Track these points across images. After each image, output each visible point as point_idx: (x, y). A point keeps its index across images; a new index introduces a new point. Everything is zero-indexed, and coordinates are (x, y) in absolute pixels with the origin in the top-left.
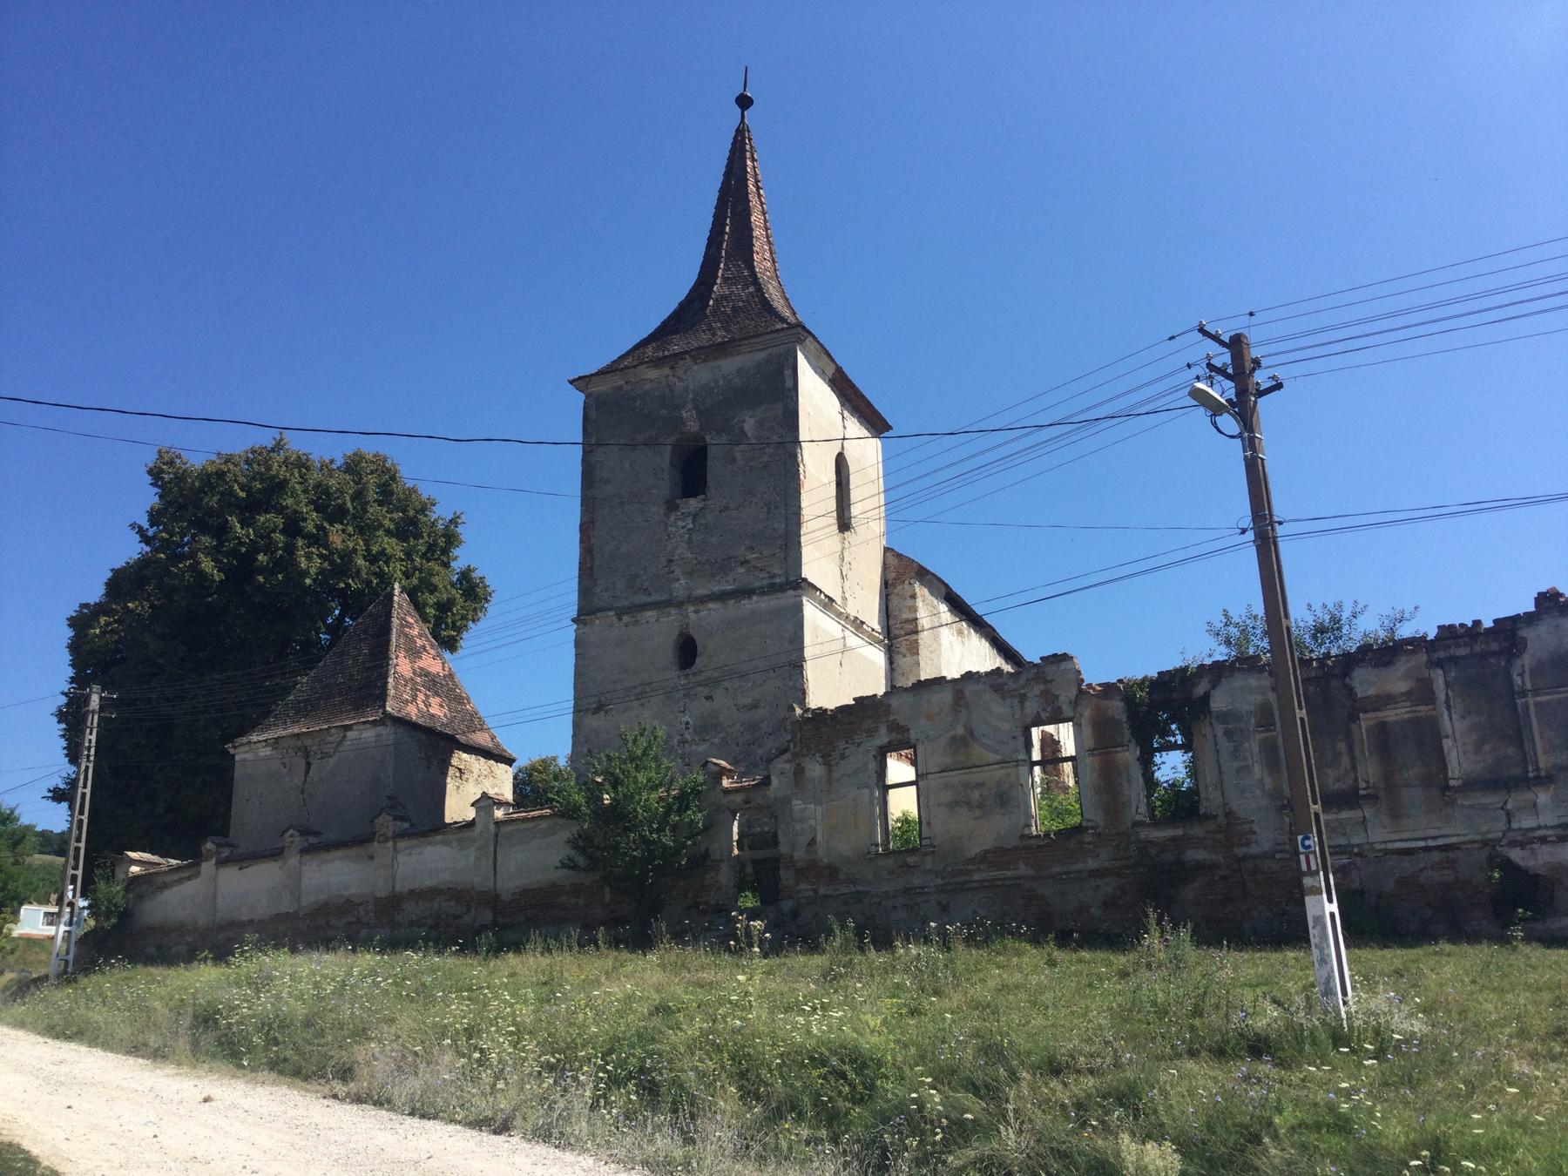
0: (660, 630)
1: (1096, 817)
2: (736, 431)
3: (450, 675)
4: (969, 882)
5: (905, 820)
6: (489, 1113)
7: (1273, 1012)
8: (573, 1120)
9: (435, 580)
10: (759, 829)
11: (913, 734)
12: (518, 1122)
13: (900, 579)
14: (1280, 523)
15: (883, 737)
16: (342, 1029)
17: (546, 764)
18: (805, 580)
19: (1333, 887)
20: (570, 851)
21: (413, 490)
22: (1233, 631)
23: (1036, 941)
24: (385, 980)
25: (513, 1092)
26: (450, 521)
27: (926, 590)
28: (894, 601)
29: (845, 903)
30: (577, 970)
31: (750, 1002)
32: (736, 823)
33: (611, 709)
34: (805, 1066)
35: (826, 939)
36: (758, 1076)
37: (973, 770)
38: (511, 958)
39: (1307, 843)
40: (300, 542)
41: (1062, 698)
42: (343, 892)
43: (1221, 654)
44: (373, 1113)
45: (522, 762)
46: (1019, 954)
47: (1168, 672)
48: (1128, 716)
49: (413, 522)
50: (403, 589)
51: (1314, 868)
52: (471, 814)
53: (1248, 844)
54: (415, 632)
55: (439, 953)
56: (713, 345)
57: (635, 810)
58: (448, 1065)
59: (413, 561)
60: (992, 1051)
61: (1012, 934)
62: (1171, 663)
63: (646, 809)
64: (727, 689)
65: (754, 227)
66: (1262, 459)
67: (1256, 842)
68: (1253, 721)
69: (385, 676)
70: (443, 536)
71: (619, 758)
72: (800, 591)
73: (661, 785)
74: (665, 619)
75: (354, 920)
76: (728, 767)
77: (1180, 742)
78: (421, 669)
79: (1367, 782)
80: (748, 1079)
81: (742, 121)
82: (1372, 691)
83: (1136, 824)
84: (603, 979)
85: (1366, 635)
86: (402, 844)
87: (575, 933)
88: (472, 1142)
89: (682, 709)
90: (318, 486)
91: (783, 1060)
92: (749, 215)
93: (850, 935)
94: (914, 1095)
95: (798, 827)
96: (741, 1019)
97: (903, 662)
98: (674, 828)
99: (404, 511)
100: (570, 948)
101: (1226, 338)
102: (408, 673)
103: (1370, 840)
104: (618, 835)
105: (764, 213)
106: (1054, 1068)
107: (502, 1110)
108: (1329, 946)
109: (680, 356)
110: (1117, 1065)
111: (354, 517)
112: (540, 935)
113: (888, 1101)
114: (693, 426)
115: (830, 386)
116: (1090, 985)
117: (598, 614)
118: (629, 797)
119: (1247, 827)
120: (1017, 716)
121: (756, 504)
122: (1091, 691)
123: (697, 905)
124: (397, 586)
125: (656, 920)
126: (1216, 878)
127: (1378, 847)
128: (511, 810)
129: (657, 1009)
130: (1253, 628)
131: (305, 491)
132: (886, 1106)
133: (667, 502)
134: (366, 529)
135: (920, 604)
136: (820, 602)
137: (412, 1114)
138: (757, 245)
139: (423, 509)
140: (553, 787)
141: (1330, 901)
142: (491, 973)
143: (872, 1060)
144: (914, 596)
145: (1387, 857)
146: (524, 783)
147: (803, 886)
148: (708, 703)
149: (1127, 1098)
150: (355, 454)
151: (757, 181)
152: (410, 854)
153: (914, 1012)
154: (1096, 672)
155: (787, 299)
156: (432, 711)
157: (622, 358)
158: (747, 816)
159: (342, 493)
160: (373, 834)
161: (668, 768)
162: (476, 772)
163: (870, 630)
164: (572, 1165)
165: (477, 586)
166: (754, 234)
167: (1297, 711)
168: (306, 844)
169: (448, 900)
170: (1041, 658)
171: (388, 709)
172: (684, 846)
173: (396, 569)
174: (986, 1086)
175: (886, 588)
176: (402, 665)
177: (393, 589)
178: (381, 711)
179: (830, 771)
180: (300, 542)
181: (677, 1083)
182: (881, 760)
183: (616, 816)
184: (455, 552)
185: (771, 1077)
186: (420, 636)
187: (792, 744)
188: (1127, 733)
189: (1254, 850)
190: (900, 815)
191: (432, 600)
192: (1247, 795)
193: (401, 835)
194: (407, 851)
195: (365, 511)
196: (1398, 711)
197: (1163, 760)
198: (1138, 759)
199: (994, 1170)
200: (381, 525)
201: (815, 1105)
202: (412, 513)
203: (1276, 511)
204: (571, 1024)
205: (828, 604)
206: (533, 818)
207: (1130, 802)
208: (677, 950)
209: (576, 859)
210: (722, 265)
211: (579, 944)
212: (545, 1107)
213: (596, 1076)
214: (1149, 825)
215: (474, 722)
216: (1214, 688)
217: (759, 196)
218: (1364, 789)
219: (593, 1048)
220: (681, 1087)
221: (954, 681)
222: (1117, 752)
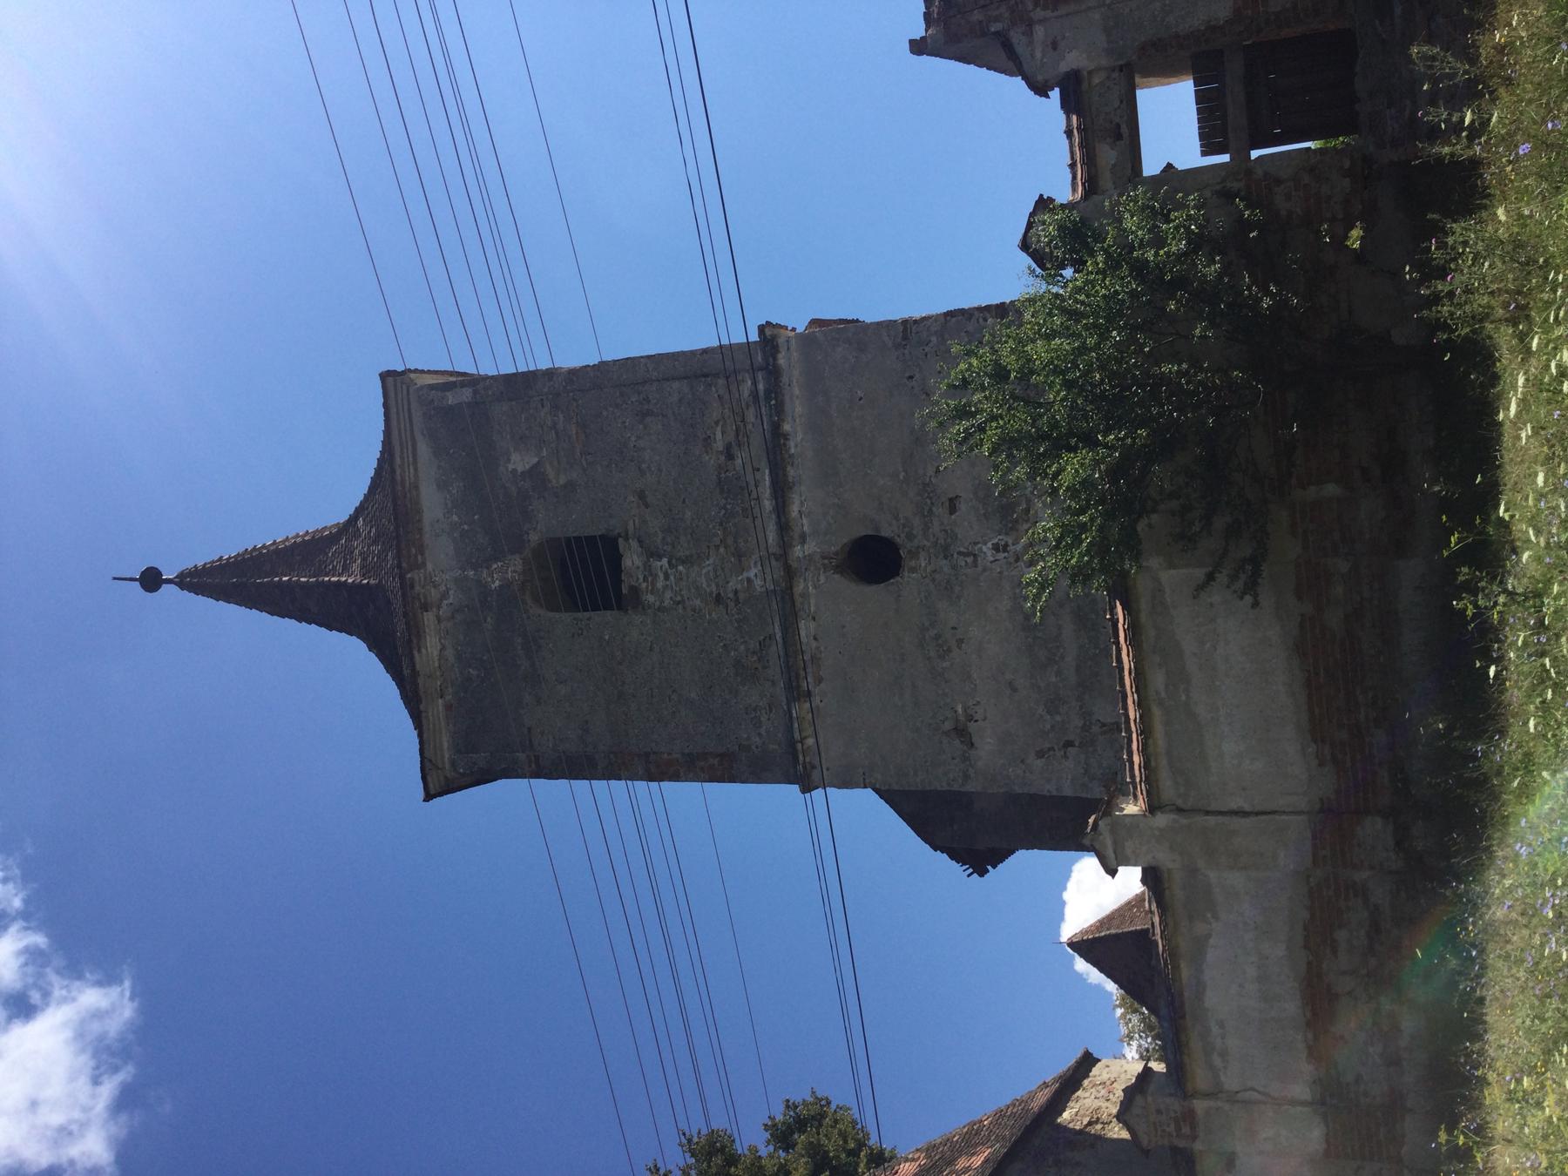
3: (928, 1150)
33: (965, 710)
74: (812, 601)
89: (970, 560)
117: (797, 736)
121: (639, 438)
148: (963, 507)
152: (1224, 1054)
160: (1175, 1150)
169: (1335, 952)
184: (741, 1148)
194: (1217, 1061)
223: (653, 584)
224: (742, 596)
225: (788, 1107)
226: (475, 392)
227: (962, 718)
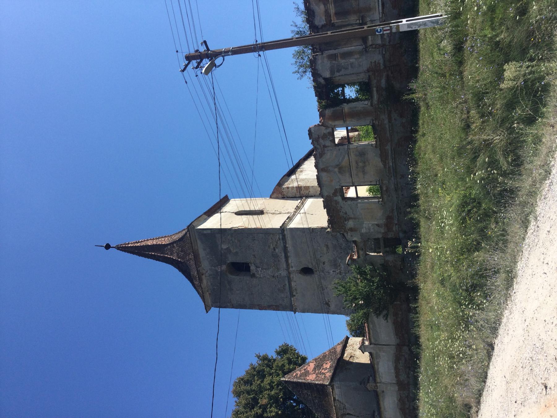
0: (299, 281)
1: (368, 120)
2: (226, 251)
3: (315, 360)
4: (393, 167)
5: (370, 190)
6: (485, 351)
7: (444, 43)
8: (489, 318)
9: (280, 365)
10: (373, 246)
11: (338, 187)
12: (489, 340)
13: (281, 193)
14: (257, 41)
15: (339, 198)
16: (449, 406)
17: (349, 325)
18: (281, 227)
19: (396, 21)
20: (381, 316)
21: (247, 372)
22: (302, 69)
23: (415, 142)
24: (430, 389)
25: (476, 342)
26: (258, 358)
27: (286, 183)
28: (290, 195)
29: (401, 213)
30: (426, 315)
31: (440, 248)
32: (370, 254)
33: (328, 300)
34: (465, 226)
35: (415, 220)
36: (469, 244)
37: (351, 165)
38: (422, 340)
39: (379, 31)
40: (265, 415)
41: (325, 132)
42: (396, 403)
43: (309, 74)
44: (484, 398)
45: (348, 333)
46: (420, 148)
47: (315, 93)
48: (332, 108)
49: (258, 372)
50: (283, 377)
51: (389, 28)
52: (367, 354)
53: (379, 63)
54: (299, 373)
55: (419, 367)
56: (195, 259)
57: (365, 291)
58: (466, 367)
59: (273, 373)
60: (460, 152)
61: (412, 151)
62: (312, 92)
63: (365, 287)
64: (321, 256)
65: (152, 244)
66: (233, 48)
67: (379, 61)
68: (334, 62)
69: (316, 385)
70: (264, 361)
71: (346, 297)
72: (285, 229)
73: (356, 282)
74: (295, 279)
75: (406, 399)
76: (349, 256)
77: (341, 89)
78: (313, 370)
79: (357, 20)
80: (471, 249)
81: (114, 247)
82: (324, 18)
83: (372, 105)
84: (430, 305)
85: (303, 21)
86: (378, 380)
87: (412, 315)
88: (498, 359)
90: (245, 408)
91: (463, 235)
92: (148, 245)
93: (413, 210)
94: (478, 181)
95: (372, 230)
96: (446, 251)
97: (312, 192)
98: (372, 277)
99: (254, 376)
100: (418, 317)
101: (187, 62)
102: (314, 376)
103: (378, 18)
104: (375, 298)
105: (148, 240)
106: (467, 127)
107: (484, 346)
108: (419, 22)
109: (198, 272)
110: (466, 102)
111: (256, 394)
112: (413, 329)
113: (480, 193)
114: (224, 267)
115: (211, 217)
116: (432, 120)
117: (293, 304)
118: (361, 294)
119: (373, 64)
120: (331, 149)
121: (253, 244)
122: (322, 121)
123: (401, 269)
124: (282, 379)
125: (407, 284)
126: (392, 75)
127: (381, 16)
128: (365, 338)
129: (442, 284)
130: (300, 63)
131: (247, 412)
132: (482, 194)
133: (252, 278)
134: (261, 390)
135: (291, 186)
136: (289, 221)
137: (485, 382)
138: (159, 243)
139: (254, 369)
140: (357, 322)
141: (402, 22)
142: (428, 348)
143: (463, 200)
144: (288, 188)
145: (385, 12)
146: (356, 333)
147: (394, 229)
148: (326, 264)
149: (479, 97)
150: (233, 393)
151: (136, 242)
152: (382, 377)
153: (444, 183)
154: (315, 119)
155: (179, 232)
156: (328, 367)
157: (199, 293)
158: (368, 250)
159: (247, 399)
161: (350, 278)
162: (351, 351)
163: (300, 204)
164: (508, 319)
165: (282, 349)
166: (155, 244)
167: (328, 35)
168: (378, 416)
169: (399, 363)
170: (310, 139)
171: (327, 384)
172: (379, 273)
173: (276, 379)
174: (475, 153)
175: (285, 198)
176: (311, 378)
177: (283, 380)
178: (328, 386)
179: (351, 218)
180: (265, 415)
181: (472, 277)
182: (347, 199)
183: (368, 298)
184: (270, 357)
185: (470, 239)
186: (300, 371)
187: (341, 232)
188: (338, 108)
189: (381, 62)
190: (368, 193)
191: (287, 366)
192: (361, 64)
193: (375, 380)
194: (381, 378)
195: (254, 390)
196: (331, 8)
197: (348, 95)
198: (348, 104)
199: (508, 150)
200: (259, 384)
201: (481, 222)
202: (255, 373)
203: (252, 43)
204: (448, 318)
205: (290, 219)
206: (369, 330)
207: (364, 107)
208: (419, 277)
209: (384, 314)
210: (166, 256)
211: (416, 314)
212: (483, 329)
213: (470, 308)
214: (372, 101)
215: (333, 351)
216: (321, 76)
217: (142, 242)
218: (359, 21)
219: (458, 309)
220: (474, 275)
221: (318, 172)
222: (345, 113)
223: (258, 273)
224: (278, 276)
225: (280, 347)
226: (211, 232)
227: (327, 301)
